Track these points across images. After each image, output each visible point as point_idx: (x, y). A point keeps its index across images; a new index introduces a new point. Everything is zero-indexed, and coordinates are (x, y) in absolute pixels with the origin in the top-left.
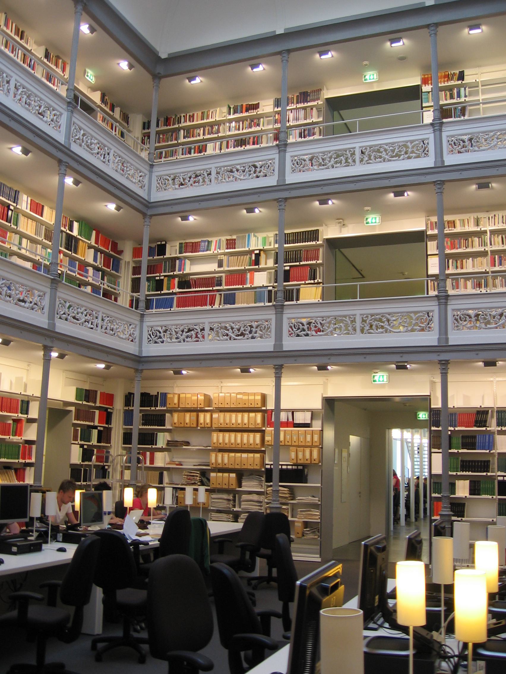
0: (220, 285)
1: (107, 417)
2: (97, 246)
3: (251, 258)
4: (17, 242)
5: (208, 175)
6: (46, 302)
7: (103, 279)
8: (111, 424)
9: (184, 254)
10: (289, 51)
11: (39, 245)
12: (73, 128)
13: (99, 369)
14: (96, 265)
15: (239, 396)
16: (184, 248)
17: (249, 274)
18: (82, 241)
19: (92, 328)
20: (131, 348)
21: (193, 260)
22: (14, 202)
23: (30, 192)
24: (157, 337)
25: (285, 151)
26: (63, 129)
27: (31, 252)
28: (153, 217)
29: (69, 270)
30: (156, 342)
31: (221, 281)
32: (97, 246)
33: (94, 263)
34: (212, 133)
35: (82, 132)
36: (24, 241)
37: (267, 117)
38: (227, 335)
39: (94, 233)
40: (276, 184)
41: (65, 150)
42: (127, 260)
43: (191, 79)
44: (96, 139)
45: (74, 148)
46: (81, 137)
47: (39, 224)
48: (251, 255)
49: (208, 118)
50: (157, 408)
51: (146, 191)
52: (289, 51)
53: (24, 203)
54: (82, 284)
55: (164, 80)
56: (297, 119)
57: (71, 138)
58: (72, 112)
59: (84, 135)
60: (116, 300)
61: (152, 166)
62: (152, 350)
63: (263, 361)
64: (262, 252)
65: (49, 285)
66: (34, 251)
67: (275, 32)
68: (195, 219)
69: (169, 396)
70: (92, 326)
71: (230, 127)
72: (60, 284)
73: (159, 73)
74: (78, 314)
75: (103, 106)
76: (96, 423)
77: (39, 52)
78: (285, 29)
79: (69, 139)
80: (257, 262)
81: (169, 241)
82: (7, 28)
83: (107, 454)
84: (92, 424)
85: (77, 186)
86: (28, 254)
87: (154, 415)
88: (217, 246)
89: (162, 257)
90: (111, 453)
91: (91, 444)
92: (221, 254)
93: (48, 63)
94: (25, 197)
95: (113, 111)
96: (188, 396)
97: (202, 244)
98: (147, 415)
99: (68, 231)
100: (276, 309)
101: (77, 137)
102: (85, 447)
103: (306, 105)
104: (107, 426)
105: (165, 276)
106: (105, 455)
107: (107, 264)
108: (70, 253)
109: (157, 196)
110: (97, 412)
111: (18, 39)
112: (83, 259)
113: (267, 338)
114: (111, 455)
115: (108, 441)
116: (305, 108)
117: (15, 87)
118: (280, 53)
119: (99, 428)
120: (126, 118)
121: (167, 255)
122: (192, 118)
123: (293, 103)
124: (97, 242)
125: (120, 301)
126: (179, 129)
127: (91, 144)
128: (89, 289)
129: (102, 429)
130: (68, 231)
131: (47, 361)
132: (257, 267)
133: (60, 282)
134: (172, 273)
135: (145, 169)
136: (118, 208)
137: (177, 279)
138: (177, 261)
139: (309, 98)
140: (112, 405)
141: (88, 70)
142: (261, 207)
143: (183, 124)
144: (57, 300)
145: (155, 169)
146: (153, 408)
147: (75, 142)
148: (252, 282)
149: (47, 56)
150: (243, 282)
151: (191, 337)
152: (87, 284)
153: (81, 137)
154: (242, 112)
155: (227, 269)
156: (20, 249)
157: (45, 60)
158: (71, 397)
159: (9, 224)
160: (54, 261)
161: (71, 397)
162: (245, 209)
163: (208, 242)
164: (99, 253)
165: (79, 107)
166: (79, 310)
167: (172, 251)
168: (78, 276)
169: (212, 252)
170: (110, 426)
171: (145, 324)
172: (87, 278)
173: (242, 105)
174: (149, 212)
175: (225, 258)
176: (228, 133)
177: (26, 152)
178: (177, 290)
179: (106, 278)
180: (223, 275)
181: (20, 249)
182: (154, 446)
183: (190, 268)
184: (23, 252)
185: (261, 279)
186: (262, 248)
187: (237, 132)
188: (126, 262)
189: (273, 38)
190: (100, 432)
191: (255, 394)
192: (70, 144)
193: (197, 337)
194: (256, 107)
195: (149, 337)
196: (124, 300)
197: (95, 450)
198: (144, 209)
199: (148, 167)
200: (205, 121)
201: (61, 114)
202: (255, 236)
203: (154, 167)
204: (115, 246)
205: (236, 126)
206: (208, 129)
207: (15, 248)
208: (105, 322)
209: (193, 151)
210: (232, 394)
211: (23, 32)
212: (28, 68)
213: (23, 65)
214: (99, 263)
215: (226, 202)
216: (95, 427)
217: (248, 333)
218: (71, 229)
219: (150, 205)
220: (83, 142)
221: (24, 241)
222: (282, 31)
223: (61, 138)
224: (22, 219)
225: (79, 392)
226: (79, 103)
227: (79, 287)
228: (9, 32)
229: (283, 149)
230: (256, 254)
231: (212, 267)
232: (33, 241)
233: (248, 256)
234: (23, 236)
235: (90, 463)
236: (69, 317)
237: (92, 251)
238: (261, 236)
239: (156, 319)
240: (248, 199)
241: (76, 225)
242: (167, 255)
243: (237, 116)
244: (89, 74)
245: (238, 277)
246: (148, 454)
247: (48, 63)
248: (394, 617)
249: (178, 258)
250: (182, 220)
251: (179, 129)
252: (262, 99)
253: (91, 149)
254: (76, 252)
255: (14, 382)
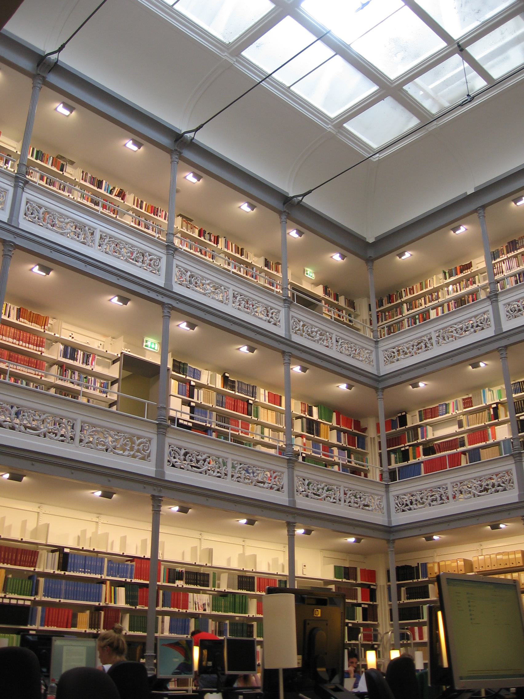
0: (463, 445)
1: (372, 594)
2: (339, 426)
3: (489, 413)
4: (259, 432)
5: (429, 339)
6: (285, 481)
7: (349, 457)
8: (375, 602)
9: (425, 421)
10: (484, 207)
11: (281, 433)
12: (291, 322)
13: (350, 544)
14: (341, 444)
15: (498, 557)
16: (423, 415)
17: (490, 429)
18: (324, 423)
19: (334, 503)
20: (379, 519)
21: (434, 426)
22: (253, 397)
23: (266, 386)
24: (406, 507)
25: (497, 301)
26: (283, 324)
27: (273, 439)
28: (386, 390)
29: (313, 452)
30: (403, 511)
31: (464, 441)
32: (339, 426)
33: (338, 443)
34: (433, 300)
35: (301, 323)
36: (266, 430)
37: (481, 274)
38: (470, 493)
39: (334, 414)
40: (494, 335)
41: (286, 341)
42: (372, 437)
43: (401, 255)
44: (317, 327)
45: (296, 338)
46: (301, 328)
47: (279, 414)
48: (489, 410)
49: (426, 287)
50: (419, 580)
51: (375, 366)
52: (484, 207)
53: (262, 396)
54: (328, 464)
55: (377, 262)
56: (510, 269)
57: (291, 330)
58: (289, 307)
59: (304, 326)
60: (366, 476)
61: (377, 342)
62: (400, 518)
63: (509, 514)
64: (499, 405)
65: (285, 465)
66: (277, 438)
67: (466, 193)
68: (426, 385)
69: (429, 565)
70: (335, 500)
71: (448, 291)
72: (296, 464)
73: (370, 257)
74: (318, 490)
75: (327, 297)
76: (360, 601)
77: (259, 263)
78: (475, 188)
79: (289, 332)
80: (496, 416)
81: (409, 411)
82: (228, 248)
83: (375, 633)
84: (355, 601)
85: (305, 372)
86: (271, 442)
87: (417, 587)
88: (455, 408)
89: (404, 427)
90: (379, 631)
91: (356, 622)
92: (460, 414)
93: (269, 270)
94: (262, 391)
95: (337, 300)
96: (447, 563)
97: (440, 408)
98: (411, 588)
99: (308, 416)
100: (514, 458)
101: (297, 329)
102: (350, 625)
103: (516, 252)
104: (371, 603)
105: (410, 446)
106: (372, 633)
107: (351, 442)
108: (313, 436)
109: (386, 369)
110: (359, 589)
111: (238, 256)
112: (327, 440)
113: (510, 489)
114: (379, 633)
115: (375, 618)
116: (515, 256)
117: (234, 297)
118: (476, 211)
119: (363, 606)
120: (351, 304)
121: (409, 425)
122: (412, 291)
123: (503, 254)
124: (338, 423)
125: (370, 477)
126: (402, 304)
127: (312, 332)
128: (336, 468)
129: (366, 606)
130: (308, 416)
131: (291, 536)
132: (497, 421)
133: (296, 461)
134: (416, 442)
135: (370, 346)
136: (349, 387)
137: (421, 447)
138: (419, 429)
139: (517, 245)
140: (375, 581)
141: (306, 269)
142: (486, 360)
143: (404, 299)
144: (296, 478)
145: (380, 344)
146: (415, 581)
147: (295, 333)
148: (494, 437)
149: (267, 264)
150: (485, 439)
151: (436, 500)
152: (334, 464)
153: (301, 328)
154: (457, 274)
155: (468, 428)
156: (262, 438)
157: (266, 269)
158: (330, 576)
159: (250, 417)
160: (288, 442)
161: (330, 576)
162: (470, 365)
163: (446, 405)
164: (342, 433)
165: (295, 303)
166: (319, 486)
167: (413, 420)
168: (323, 457)
169: (450, 414)
170: (375, 603)
171: (391, 494)
172: (332, 457)
173: (456, 268)
174: (381, 386)
175: (463, 418)
176: (447, 297)
177: (251, 349)
178: (422, 458)
179: (352, 456)
180: (465, 435)
181: (262, 438)
182: (421, 620)
183: (431, 434)
184: (266, 440)
185: (503, 433)
186: (498, 401)
187: (456, 294)
188: (371, 438)
189: (466, 199)
190: (364, 609)
191: (514, 553)
192: (290, 336)
193: (441, 499)
194: (469, 266)
195: (397, 506)
196: (375, 475)
197: (362, 628)
198: (375, 385)
199: (373, 345)
200: (425, 290)
201: (279, 312)
202: (490, 390)
203: (379, 343)
204: (357, 425)
205: (453, 289)
206: (429, 298)
207: (258, 438)
208: (348, 496)
209: (417, 321)
210: (492, 556)
211: (242, 249)
212: (251, 278)
213: (247, 276)
214: (344, 442)
215: (449, 362)
216: (359, 605)
217: (490, 487)
218: (311, 414)
219: (380, 379)
220: (304, 332)
221: (266, 430)
222: (472, 191)
223: (280, 331)
224: (262, 411)
225: (337, 569)
226: (306, 301)
227: (326, 466)
228: (229, 252)
229: (494, 299)
230: (493, 408)
231: (453, 429)
232: (275, 429)
233: (487, 412)
234: (264, 426)
235: (357, 642)
236: (309, 494)
237: (335, 432)
238: (495, 390)
239: (402, 489)
240: (471, 355)
241: (315, 410)
242: (409, 425)
243: (453, 279)
244: (308, 272)
245: (480, 434)
246: (416, 629)
247: (269, 270)
248: (440, 664)
249: (419, 426)
250: (413, 388)
251: (402, 304)
252: (473, 259)
253: (313, 337)
254: (318, 435)
255: (271, 563)
